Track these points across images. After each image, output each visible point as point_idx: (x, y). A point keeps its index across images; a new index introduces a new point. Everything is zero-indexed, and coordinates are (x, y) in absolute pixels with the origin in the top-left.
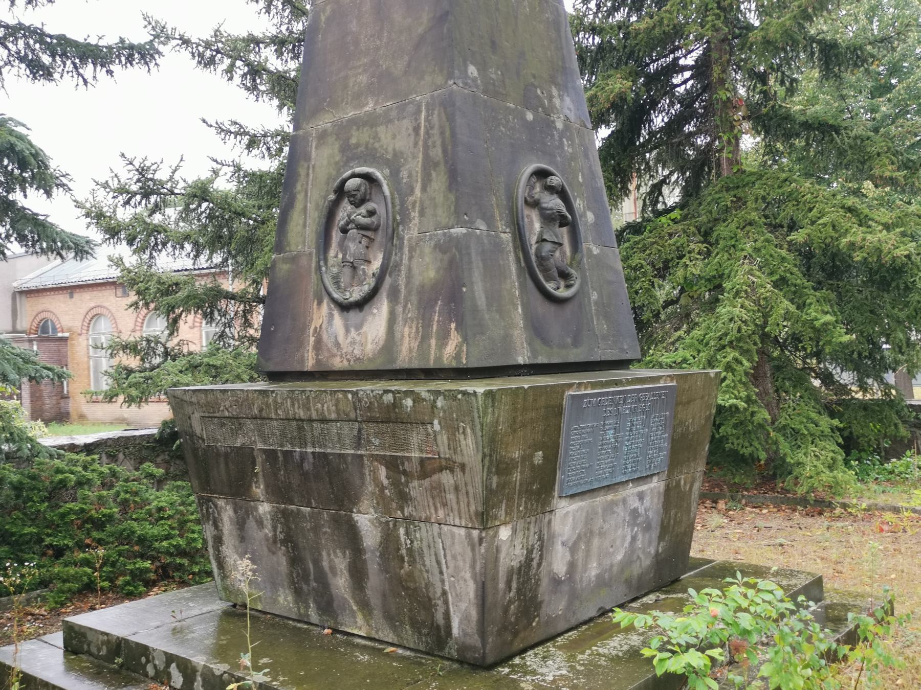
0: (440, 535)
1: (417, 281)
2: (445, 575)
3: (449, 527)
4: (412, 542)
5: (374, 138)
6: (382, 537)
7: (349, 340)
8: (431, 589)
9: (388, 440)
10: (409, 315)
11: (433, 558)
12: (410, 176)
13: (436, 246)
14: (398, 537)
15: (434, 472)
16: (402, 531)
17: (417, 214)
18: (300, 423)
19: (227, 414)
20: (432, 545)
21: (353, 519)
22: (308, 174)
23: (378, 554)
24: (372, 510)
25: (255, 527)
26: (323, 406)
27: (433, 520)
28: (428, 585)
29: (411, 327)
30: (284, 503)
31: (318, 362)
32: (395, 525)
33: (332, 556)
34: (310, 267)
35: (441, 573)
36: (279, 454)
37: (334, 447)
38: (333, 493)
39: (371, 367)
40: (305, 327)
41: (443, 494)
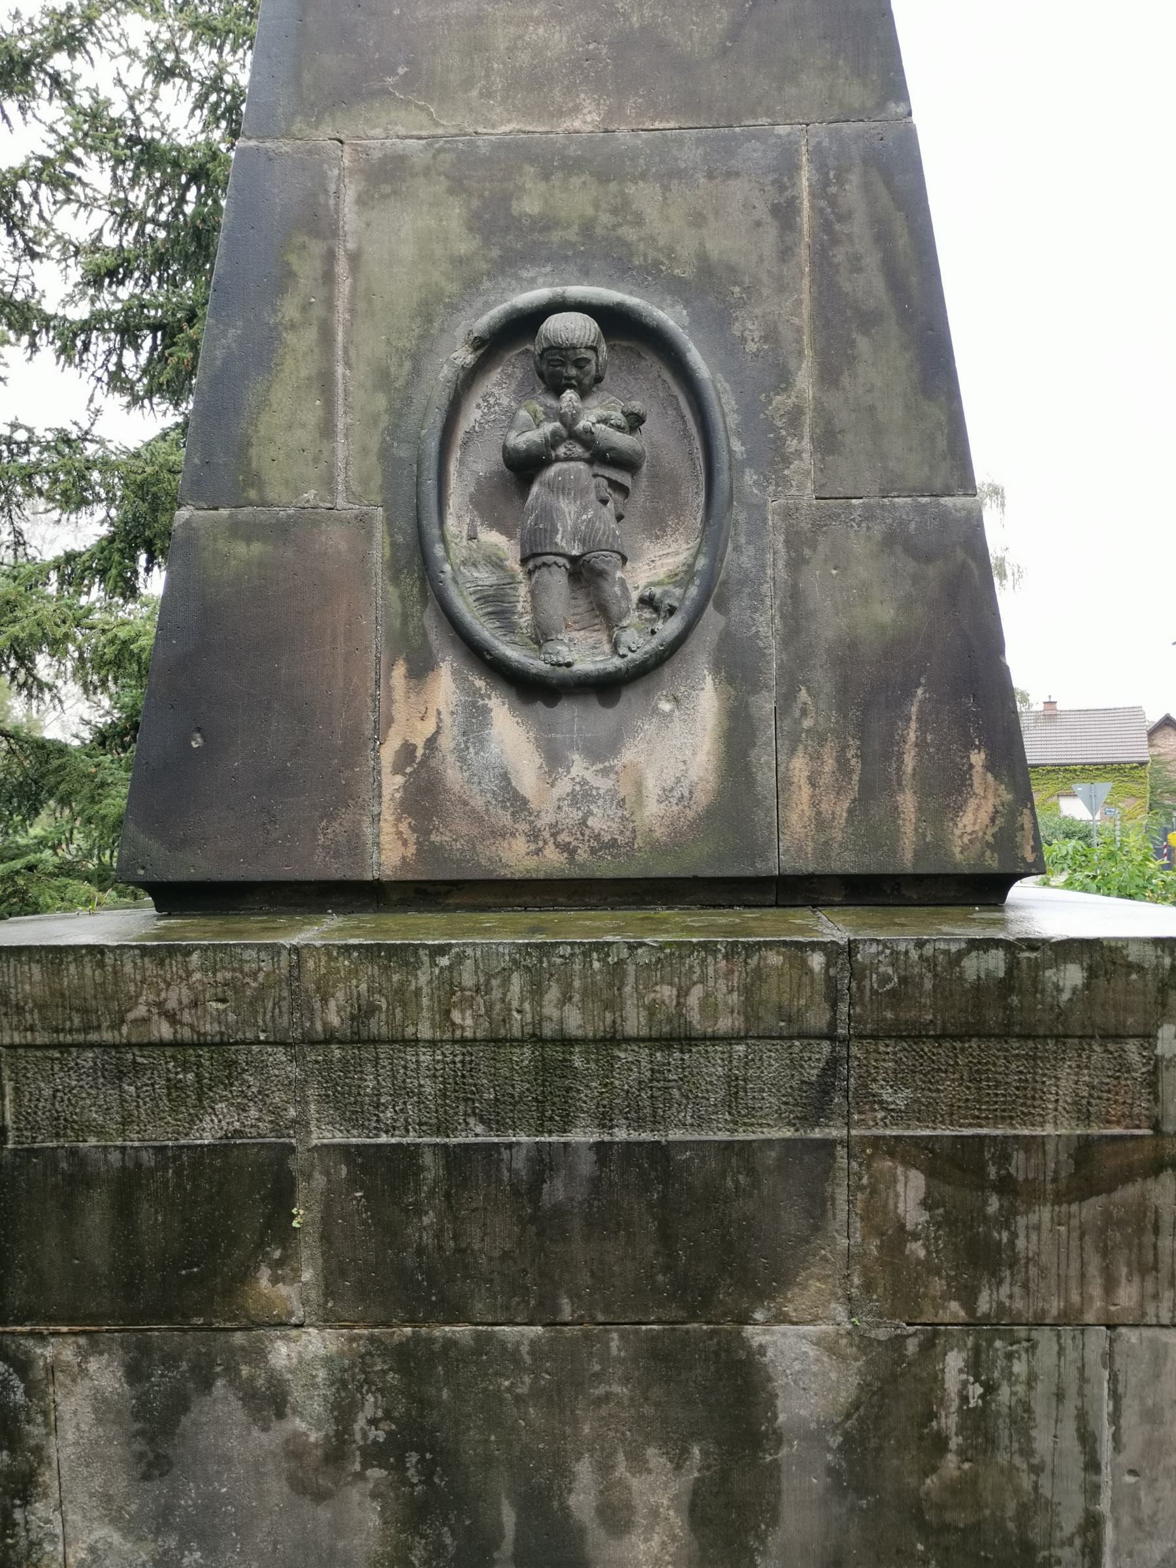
0: (1109, 1358)
1: (828, 626)
2: (1106, 1471)
3: (1147, 1333)
4: (990, 1388)
5: (615, 211)
6: (863, 1387)
7: (564, 786)
8: (1040, 1521)
9: (949, 1089)
10: (807, 723)
11: (1069, 1429)
12: (771, 335)
13: (890, 540)
14: (937, 1380)
15: (1127, 1176)
16: (954, 1362)
17: (807, 444)
18: (555, 1053)
19: (165, 1031)
20: (1072, 1390)
21: (743, 1343)
22: (329, 277)
23: (835, 1441)
24: (839, 1310)
25: (241, 1415)
26: (683, 993)
27: (1089, 1317)
28: (1034, 1506)
29: (816, 757)
30: (412, 1321)
31: (427, 851)
32: (928, 1346)
33: (621, 1469)
34: (364, 559)
35: (1093, 1466)
36: (428, 1159)
37: (701, 1122)
38: (666, 1269)
39: (666, 869)
40: (357, 745)
41: (1148, 1239)
